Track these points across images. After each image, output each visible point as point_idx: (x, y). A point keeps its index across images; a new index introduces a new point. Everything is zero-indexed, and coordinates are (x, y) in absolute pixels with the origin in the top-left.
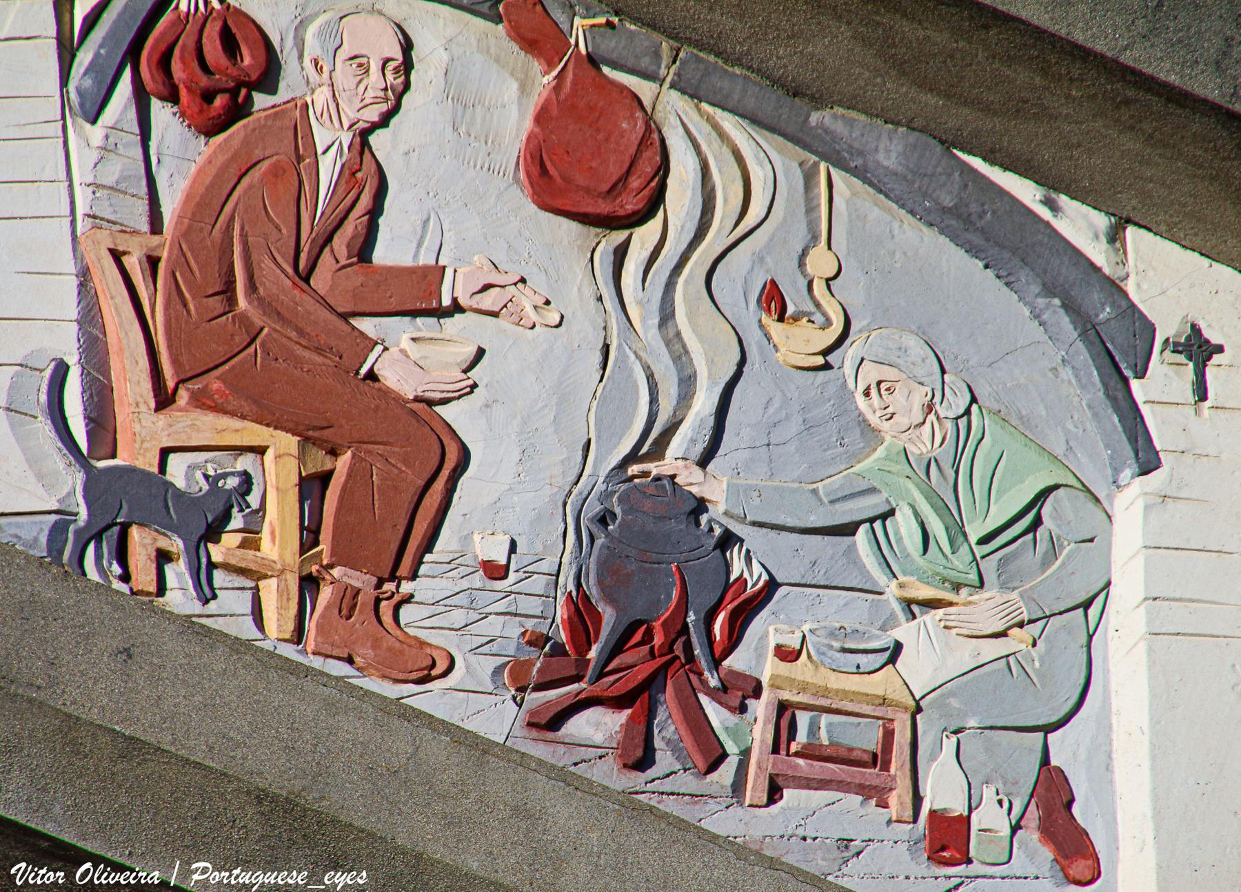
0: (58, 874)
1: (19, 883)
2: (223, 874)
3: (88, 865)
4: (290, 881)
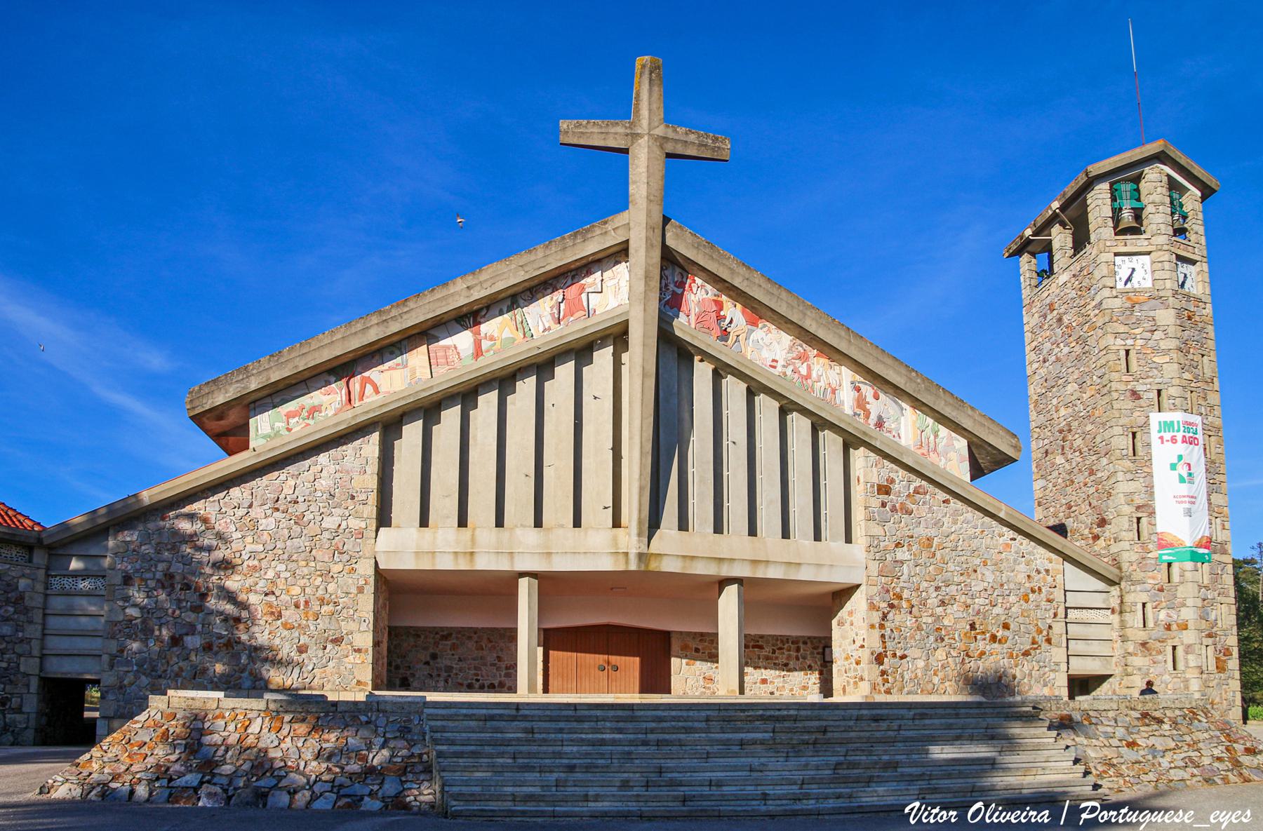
0: (951, 813)
1: (913, 822)
2: (1111, 813)
3: (979, 805)
4: (1177, 821)
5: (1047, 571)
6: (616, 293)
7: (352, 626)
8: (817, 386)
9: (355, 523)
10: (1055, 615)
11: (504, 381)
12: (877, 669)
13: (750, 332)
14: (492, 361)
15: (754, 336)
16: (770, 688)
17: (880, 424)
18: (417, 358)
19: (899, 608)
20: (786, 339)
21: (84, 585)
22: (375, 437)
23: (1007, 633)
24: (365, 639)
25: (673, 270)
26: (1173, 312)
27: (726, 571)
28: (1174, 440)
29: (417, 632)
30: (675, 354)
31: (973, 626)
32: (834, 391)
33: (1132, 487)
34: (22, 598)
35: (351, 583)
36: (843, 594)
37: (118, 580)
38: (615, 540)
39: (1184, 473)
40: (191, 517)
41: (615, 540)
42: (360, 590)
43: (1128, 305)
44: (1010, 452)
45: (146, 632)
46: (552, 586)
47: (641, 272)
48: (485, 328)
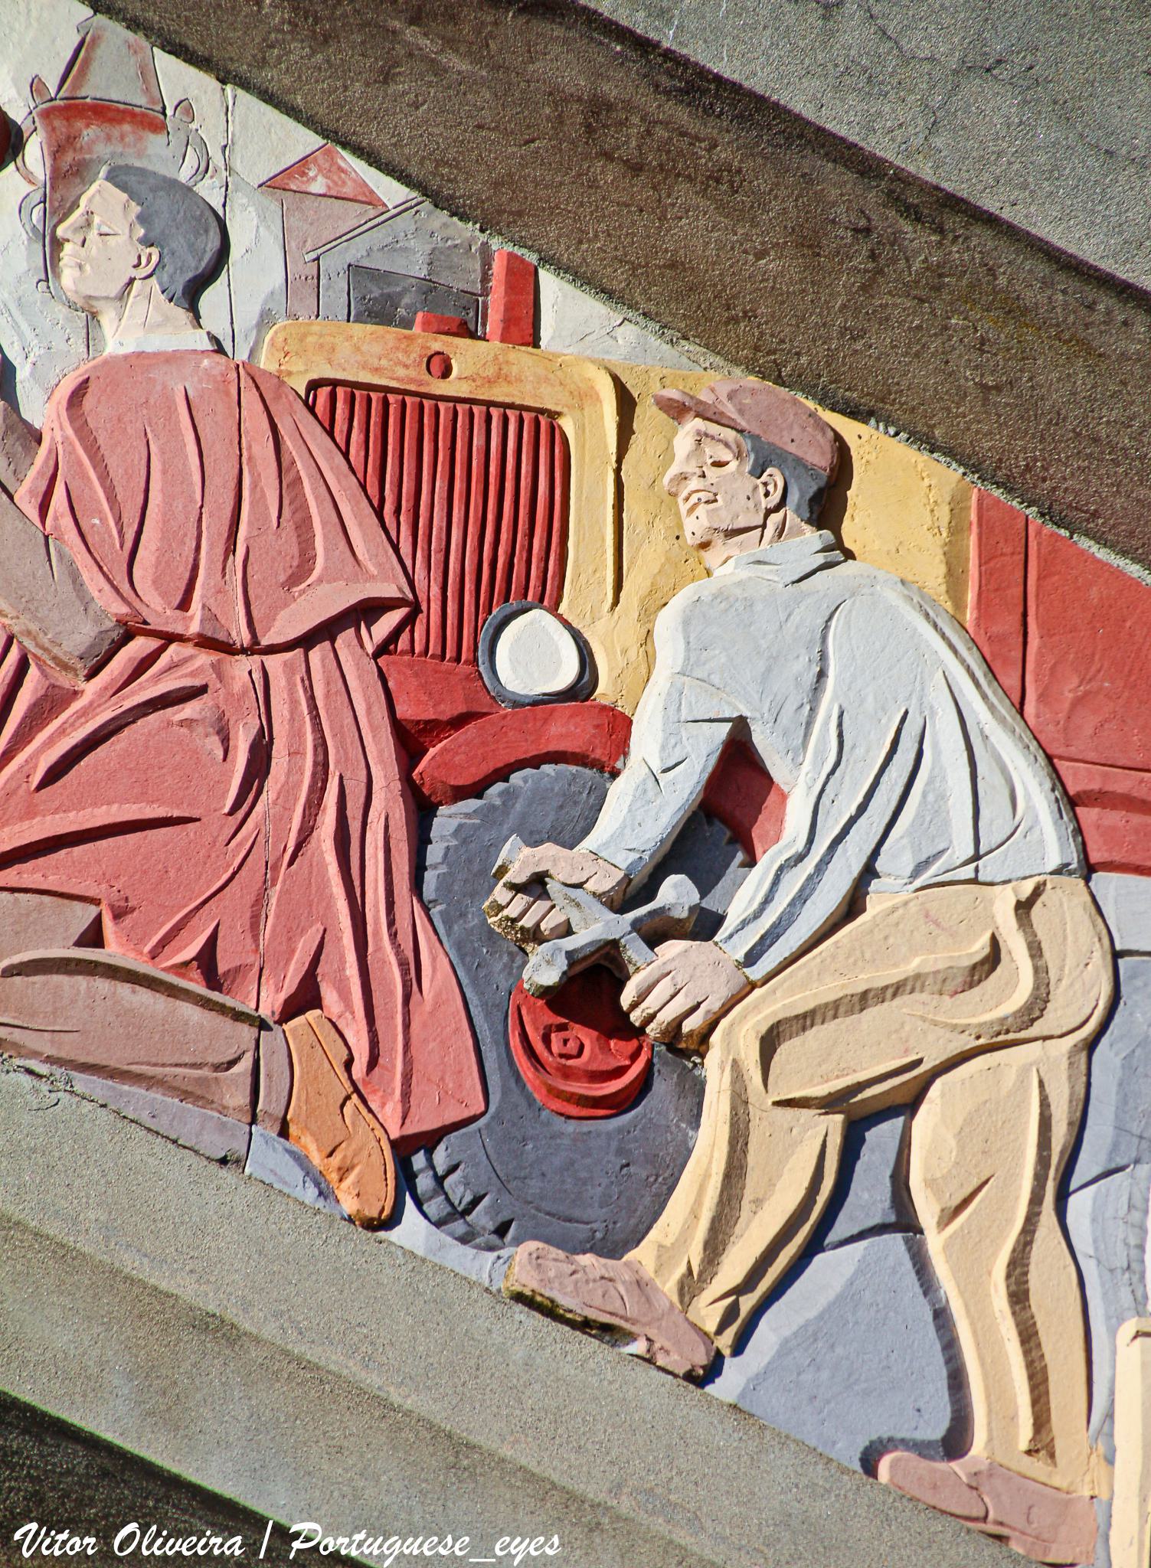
0: (87, 1540)
1: (26, 1555)
3: (132, 1527)
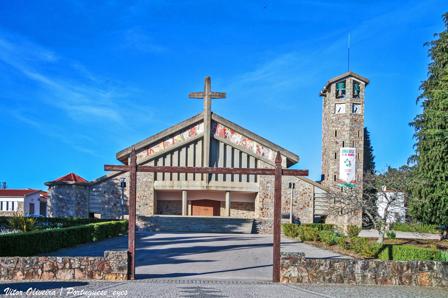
5: (309, 189)
6: (201, 130)
7: (150, 201)
8: (248, 147)
9: (150, 180)
10: (311, 199)
11: (179, 149)
12: (261, 212)
13: (232, 135)
14: (176, 145)
15: (233, 136)
16: (245, 215)
17: (263, 155)
18: (161, 145)
19: (267, 198)
20: (241, 136)
21: (96, 194)
22: (153, 161)
23: (296, 204)
24: (152, 204)
25: (213, 125)
26: (349, 120)
27: (226, 189)
28: (346, 155)
29: (164, 201)
30: (214, 143)
31: (287, 202)
32: (252, 148)
33: (334, 167)
34: (85, 196)
35: (149, 192)
36: (256, 193)
37: (103, 192)
38: (201, 184)
39: (348, 163)
40: (117, 179)
41: (201, 184)
42: (151, 194)
43: (337, 118)
44: (296, 160)
45: (109, 204)
46: (190, 193)
47: (206, 126)
48: (175, 138)
